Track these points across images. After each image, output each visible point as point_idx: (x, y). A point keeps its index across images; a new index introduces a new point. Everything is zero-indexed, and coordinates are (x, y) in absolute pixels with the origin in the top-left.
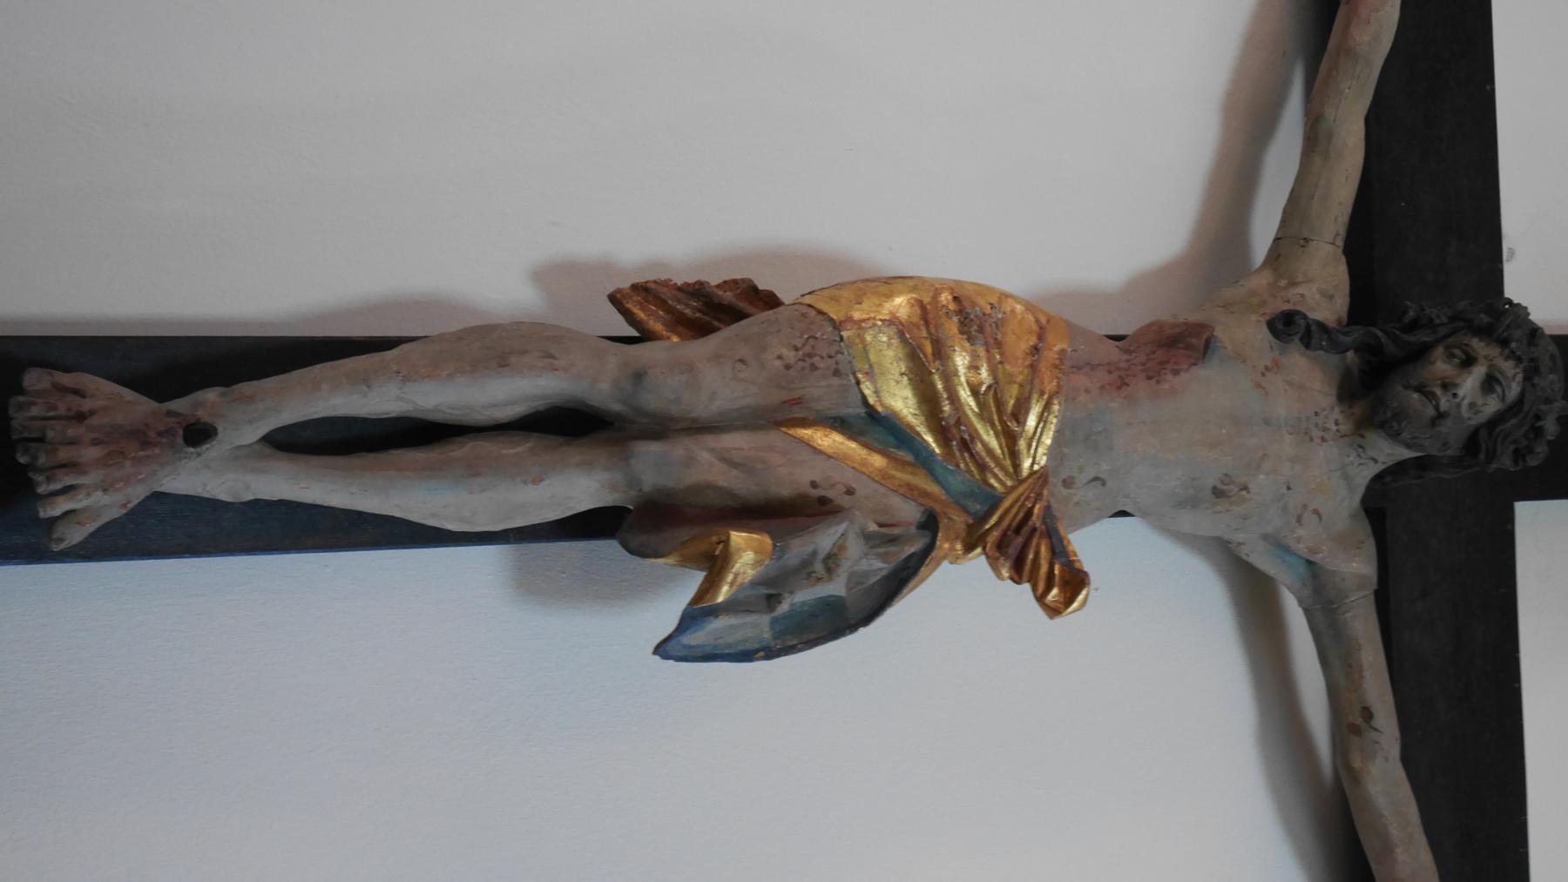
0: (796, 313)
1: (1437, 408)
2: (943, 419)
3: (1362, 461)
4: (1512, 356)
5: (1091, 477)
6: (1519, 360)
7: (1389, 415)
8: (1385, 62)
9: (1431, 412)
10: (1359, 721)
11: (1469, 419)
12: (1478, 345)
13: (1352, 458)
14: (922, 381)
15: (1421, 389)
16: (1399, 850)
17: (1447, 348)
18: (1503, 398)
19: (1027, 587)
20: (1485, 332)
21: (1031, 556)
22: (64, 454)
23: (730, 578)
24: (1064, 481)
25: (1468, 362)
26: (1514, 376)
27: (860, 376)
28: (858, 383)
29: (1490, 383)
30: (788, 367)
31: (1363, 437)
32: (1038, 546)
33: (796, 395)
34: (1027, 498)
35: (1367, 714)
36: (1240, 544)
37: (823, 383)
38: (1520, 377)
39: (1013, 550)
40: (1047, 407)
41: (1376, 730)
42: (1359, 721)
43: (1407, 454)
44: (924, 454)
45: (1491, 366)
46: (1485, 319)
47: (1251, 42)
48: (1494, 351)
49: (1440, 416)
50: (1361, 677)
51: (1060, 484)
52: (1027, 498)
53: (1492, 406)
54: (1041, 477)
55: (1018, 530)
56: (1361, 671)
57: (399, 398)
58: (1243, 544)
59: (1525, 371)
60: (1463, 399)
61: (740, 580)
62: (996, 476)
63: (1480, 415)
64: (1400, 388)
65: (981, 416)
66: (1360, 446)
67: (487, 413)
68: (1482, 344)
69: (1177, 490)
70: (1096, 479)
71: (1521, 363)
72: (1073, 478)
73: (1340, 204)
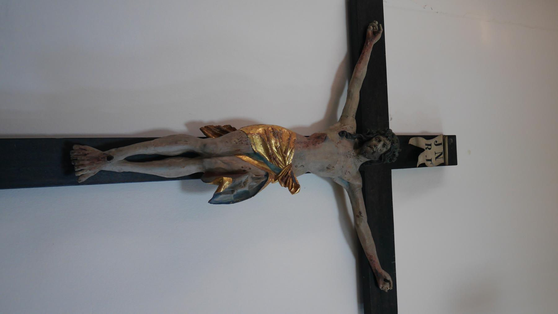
1: (373, 150)
6: (390, 140)
7: (364, 152)
9: (372, 151)
10: (359, 214)
12: (382, 138)
15: (370, 147)
17: (375, 138)
19: (287, 188)
20: (383, 135)
21: (288, 182)
22: (81, 163)
23: (223, 187)
25: (380, 141)
28: (252, 146)
29: (384, 145)
30: (237, 143)
31: (359, 156)
32: (290, 179)
34: (268, 134)
38: (390, 144)
39: (284, 180)
40: (291, 151)
42: (359, 214)
46: (383, 132)
47: (337, 75)
48: (385, 139)
49: (374, 152)
50: (359, 205)
52: (268, 134)
53: (385, 150)
54: (290, 165)
56: (359, 204)
59: (391, 143)
61: (225, 187)
62: (281, 165)
64: (366, 146)
68: (383, 137)
70: (302, 166)
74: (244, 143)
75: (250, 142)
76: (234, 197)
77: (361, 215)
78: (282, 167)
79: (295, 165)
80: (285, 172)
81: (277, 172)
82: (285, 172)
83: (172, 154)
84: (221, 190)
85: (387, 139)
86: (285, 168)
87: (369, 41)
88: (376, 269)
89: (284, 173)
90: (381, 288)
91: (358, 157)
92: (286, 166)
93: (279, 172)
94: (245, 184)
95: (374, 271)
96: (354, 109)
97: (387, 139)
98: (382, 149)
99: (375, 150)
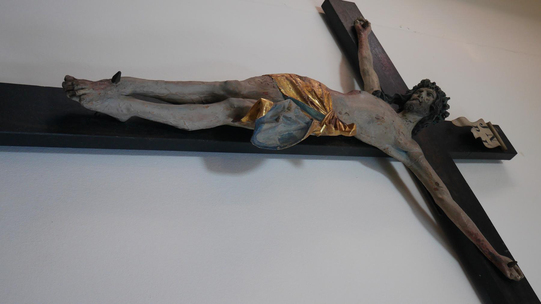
0: (259, 82)
1: (419, 101)
2: (304, 97)
3: (408, 123)
4: (431, 88)
5: (345, 113)
7: (409, 105)
8: (374, 34)
10: (436, 187)
11: (428, 102)
13: (405, 122)
14: (296, 89)
16: (461, 214)
18: (433, 97)
21: (338, 124)
22: (79, 87)
23: (265, 109)
24: (339, 113)
26: (433, 91)
27: (280, 88)
28: (280, 90)
29: (429, 94)
30: (262, 83)
31: (405, 116)
32: (339, 123)
33: (266, 91)
35: (437, 184)
36: (387, 148)
37: (272, 89)
38: (435, 92)
41: (441, 187)
42: (436, 187)
43: (418, 118)
44: (302, 105)
45: (427, 91)
47: (341, 74)
48: (426, 89)
49: (421, 103)
50: (431, 175)
51: (338, 113)
53: (431, 99)
55: (332, 119)
56: (431, 174)
57: (166, 88)
58: (388, 148)
59: (435, 90)
60: (424, 98)
61: (267, 109)
62: (322, 111)
63: (430, 101)
65: (313, 98)
66: (406, 118)
67: (189, 97)
69: (367, 118)
70: (346, 113)
71: (434, 89)
72: (340, 111)
73: (376, 81)
74: (270, 84)
75: (276, 85)
76: (279, 142)
77: (439, 186)
78: (325, 113)
79: (338, 112)
80: (330, 116)
81: (321, 118)
82: (330, 116)
83: (188, 98)
84: (263, 115)
85: (429, 88)
86: (327, 114)
87: (361, 32)
88: (491, 251)
89: (329, 118)
90: (509, 275)
91: (405, 117)
92: (328, 113)
93: (322, 119)
94: (289, 108)
95: (489, 257)
96: (376, 81)
97: (429, 88)
98: (428, 98)
99: (421, 101)
